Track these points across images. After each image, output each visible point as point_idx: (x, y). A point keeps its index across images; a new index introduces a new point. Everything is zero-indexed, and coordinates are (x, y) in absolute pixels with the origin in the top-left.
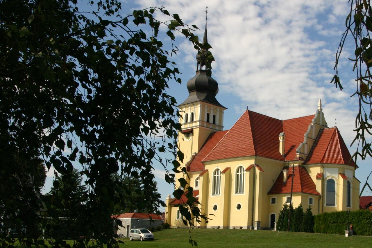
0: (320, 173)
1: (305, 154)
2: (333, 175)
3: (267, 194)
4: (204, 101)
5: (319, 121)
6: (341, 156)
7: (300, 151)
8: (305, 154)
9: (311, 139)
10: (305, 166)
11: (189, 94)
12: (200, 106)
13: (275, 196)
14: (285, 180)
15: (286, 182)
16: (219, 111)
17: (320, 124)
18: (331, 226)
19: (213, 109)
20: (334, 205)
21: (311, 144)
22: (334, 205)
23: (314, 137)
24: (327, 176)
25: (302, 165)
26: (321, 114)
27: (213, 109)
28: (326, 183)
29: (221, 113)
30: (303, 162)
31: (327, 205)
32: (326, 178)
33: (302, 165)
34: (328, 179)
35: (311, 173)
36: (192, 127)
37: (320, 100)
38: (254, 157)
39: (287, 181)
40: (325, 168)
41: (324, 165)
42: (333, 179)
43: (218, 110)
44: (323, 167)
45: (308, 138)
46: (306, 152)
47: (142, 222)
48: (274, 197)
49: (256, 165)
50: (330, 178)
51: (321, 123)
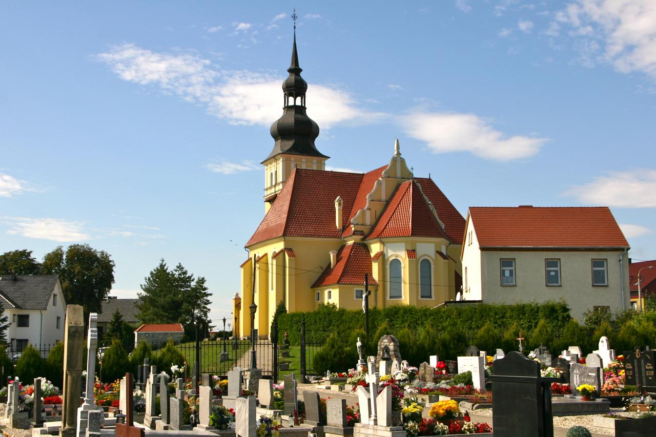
0: (379, 251)
1: (365, 225)
2: (397, 253)
3: (310, 287)
4: (288, 152)
5: (396, 173)
6: (410, 223)
7: (356, 222)
8: (365, 225)
9: (380, 201)
10: (365, 242)
11: (274, 142)
12: (283, 161)
13: (318, 290)
14: (332, 267)
15: (333, 269)
16: (317, 163)
17: (398, 177)
18: (288, 325)
19: (306, 162)
20: (401, 296)
21: (379, 207)
22: (401, 297)
23: (384, 197)
24: (389, 255)
25: (361, 242)
26: (397, 162)
27: (306, 162)
28: (388, 267)
29: (321, 165)
30: (361, 237)
31: (391, 297)
32: (388, 258)
33: (361, 242)
34: (391, 259)
35: (372, 252)
36: (275, 192)
37: (397, 140)
38: (283, 238)
39: (334, 267)
40: (386, 244)
41: (383, 240)
42: (398, 258)
43: (315, 161)
44: (383, 243)
45: (372, 200)
46: (368, 221)
47: (153, 336)
48: (330, 290)
49: (288, 249)
50: (394, 258)
51: (399, 174)
